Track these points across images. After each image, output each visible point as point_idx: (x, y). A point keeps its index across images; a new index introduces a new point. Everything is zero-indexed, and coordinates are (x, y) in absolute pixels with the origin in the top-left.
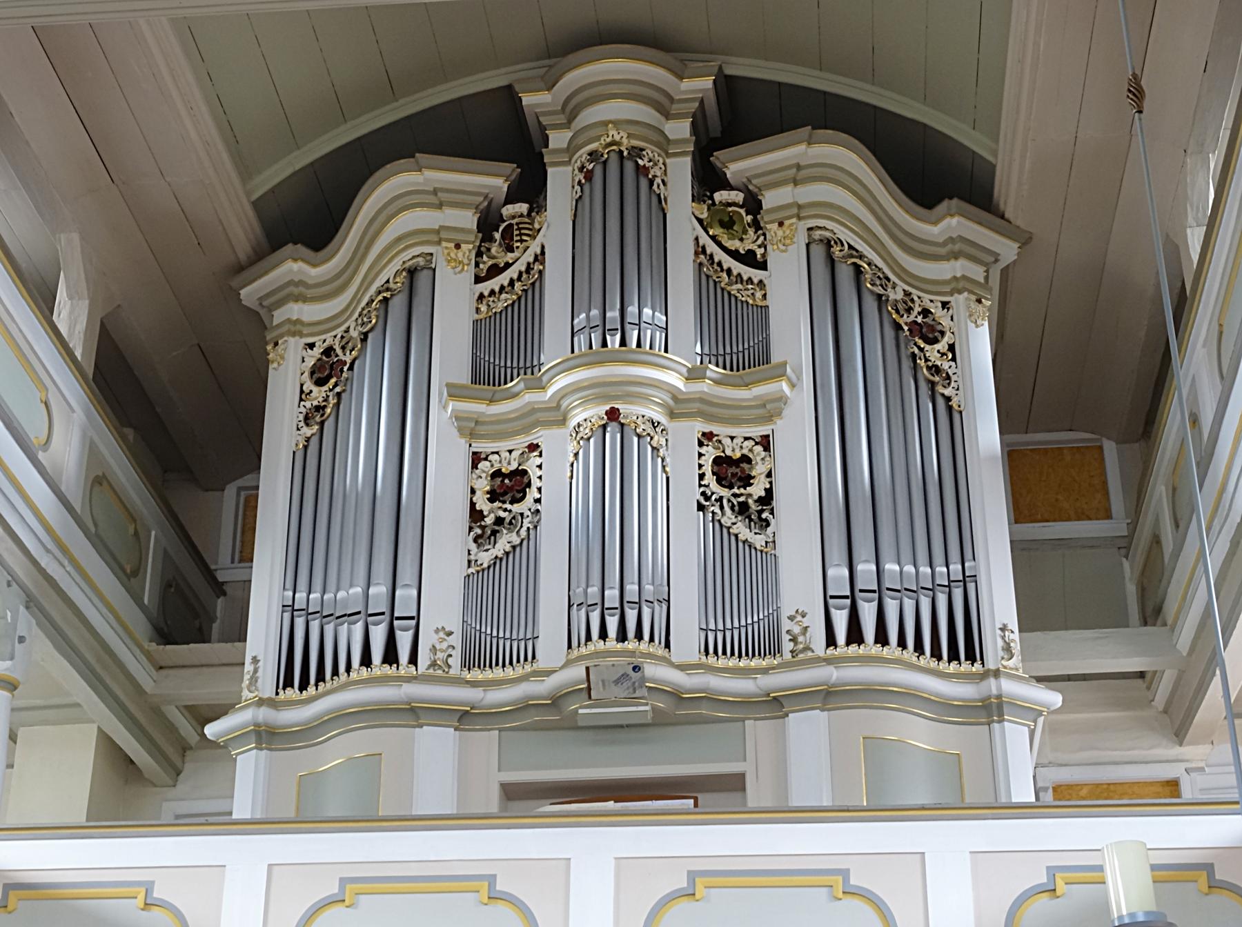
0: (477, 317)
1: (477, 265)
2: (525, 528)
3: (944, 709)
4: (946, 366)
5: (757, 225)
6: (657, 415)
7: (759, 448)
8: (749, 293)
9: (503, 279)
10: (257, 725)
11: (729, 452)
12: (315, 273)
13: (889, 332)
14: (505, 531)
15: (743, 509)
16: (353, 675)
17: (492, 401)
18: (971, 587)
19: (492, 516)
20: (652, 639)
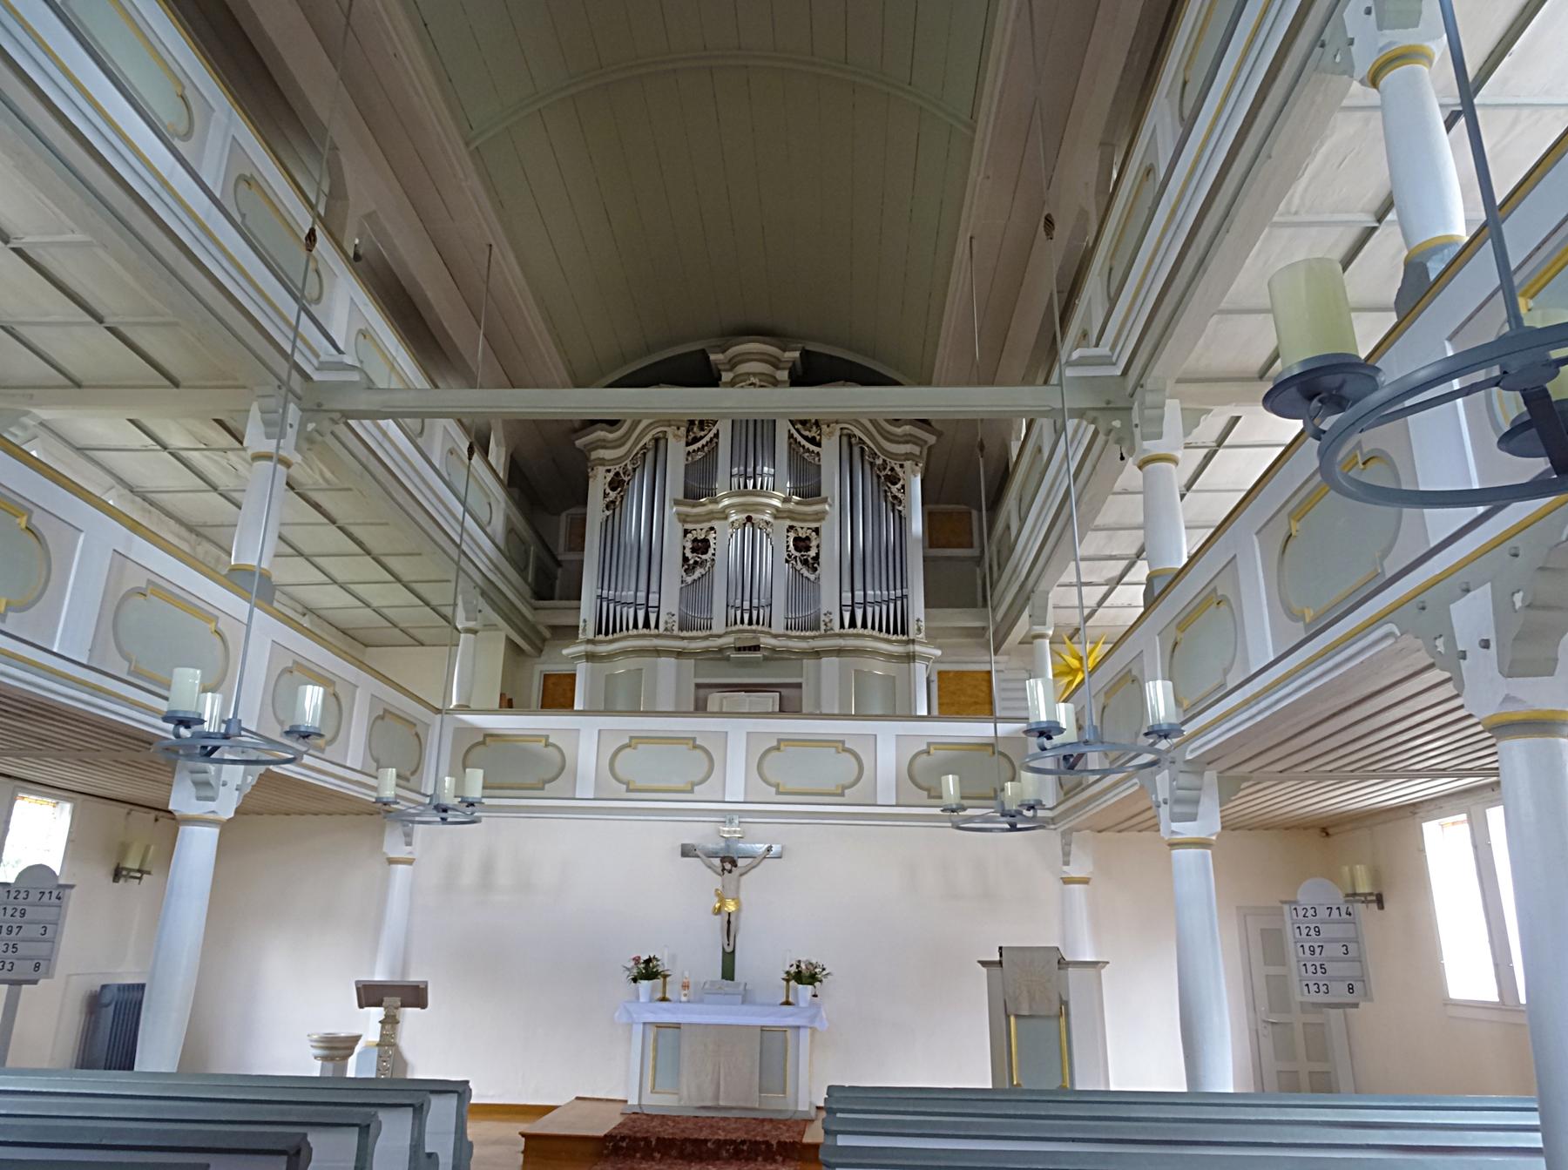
3: (890, 656)
4: (900, 495)
6: (767, 518)
7: (814, 534)
9: (699, 445)
12: (611, 436)
15: (805, 562)
16: (630, 632)
17: (694, 506)
18: (905, 600)
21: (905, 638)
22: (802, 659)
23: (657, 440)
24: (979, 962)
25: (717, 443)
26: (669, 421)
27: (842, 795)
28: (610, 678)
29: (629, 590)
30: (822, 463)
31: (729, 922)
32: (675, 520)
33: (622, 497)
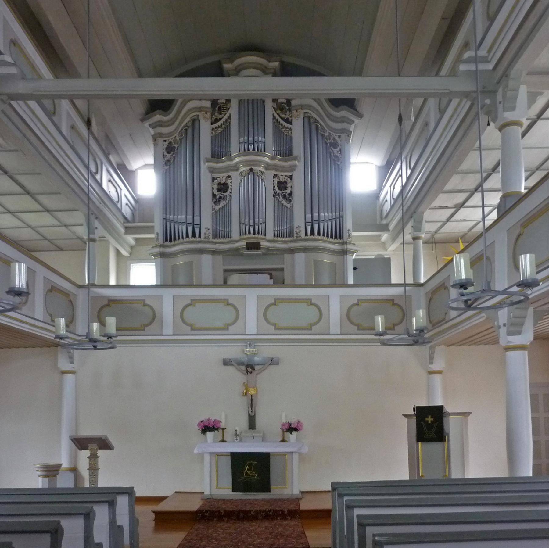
0: (212, 135)
1: (211, 118)
2: (227, 200)
3: (333, 252)
4: (338, 155)
5: (290, 110)
6: (262, 169)
7: (289, 179)
8: (287, 131)
9: (219, 123)
10: (160, 252)
11: (281, 180)
12: (165, 119)
13: (324, 145)
14: (222, 201)
15: (284, 197)
16: (185, 240)
17: (218, 163)
18: (341, 219)
19: (218, 196)
20: (262, 234)
21: (341, 241)
22: (283, 254)
23: (193, 121)
24: (403, 415)
25: (230, 123)
26: (200, 108)
27: (311, 329)
28: (174, 268)
29: (181, 215)
30: (294, 135)
31: (252, 400)
32: (207, 171)
33: (174, 157)
